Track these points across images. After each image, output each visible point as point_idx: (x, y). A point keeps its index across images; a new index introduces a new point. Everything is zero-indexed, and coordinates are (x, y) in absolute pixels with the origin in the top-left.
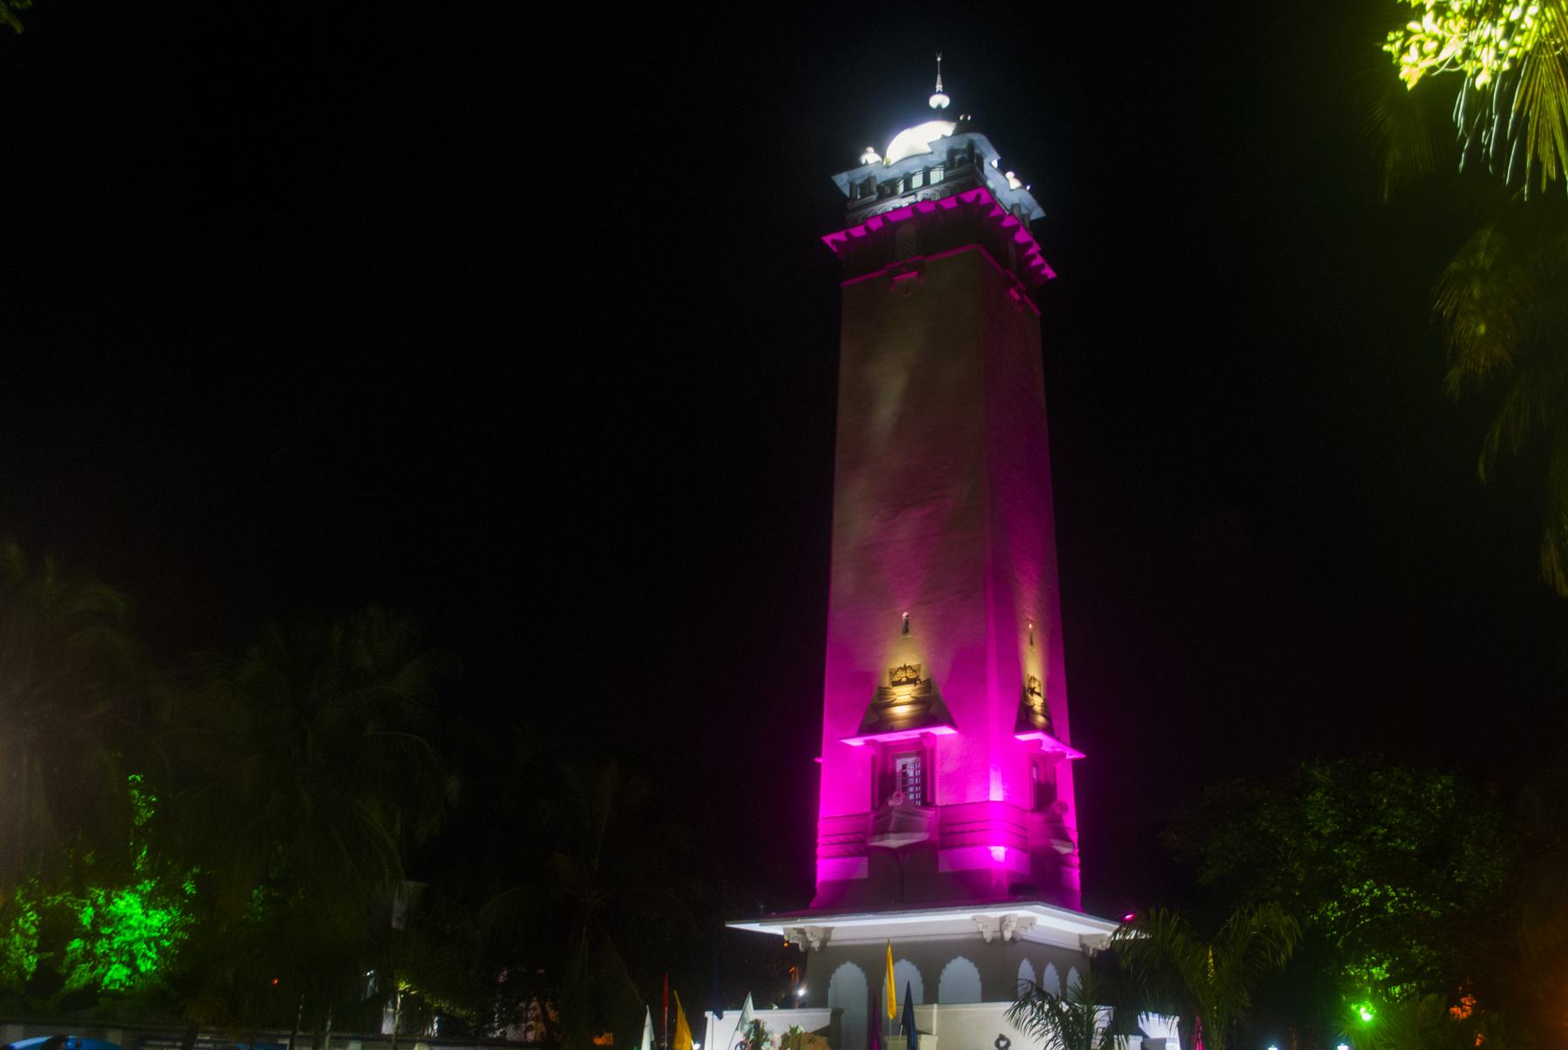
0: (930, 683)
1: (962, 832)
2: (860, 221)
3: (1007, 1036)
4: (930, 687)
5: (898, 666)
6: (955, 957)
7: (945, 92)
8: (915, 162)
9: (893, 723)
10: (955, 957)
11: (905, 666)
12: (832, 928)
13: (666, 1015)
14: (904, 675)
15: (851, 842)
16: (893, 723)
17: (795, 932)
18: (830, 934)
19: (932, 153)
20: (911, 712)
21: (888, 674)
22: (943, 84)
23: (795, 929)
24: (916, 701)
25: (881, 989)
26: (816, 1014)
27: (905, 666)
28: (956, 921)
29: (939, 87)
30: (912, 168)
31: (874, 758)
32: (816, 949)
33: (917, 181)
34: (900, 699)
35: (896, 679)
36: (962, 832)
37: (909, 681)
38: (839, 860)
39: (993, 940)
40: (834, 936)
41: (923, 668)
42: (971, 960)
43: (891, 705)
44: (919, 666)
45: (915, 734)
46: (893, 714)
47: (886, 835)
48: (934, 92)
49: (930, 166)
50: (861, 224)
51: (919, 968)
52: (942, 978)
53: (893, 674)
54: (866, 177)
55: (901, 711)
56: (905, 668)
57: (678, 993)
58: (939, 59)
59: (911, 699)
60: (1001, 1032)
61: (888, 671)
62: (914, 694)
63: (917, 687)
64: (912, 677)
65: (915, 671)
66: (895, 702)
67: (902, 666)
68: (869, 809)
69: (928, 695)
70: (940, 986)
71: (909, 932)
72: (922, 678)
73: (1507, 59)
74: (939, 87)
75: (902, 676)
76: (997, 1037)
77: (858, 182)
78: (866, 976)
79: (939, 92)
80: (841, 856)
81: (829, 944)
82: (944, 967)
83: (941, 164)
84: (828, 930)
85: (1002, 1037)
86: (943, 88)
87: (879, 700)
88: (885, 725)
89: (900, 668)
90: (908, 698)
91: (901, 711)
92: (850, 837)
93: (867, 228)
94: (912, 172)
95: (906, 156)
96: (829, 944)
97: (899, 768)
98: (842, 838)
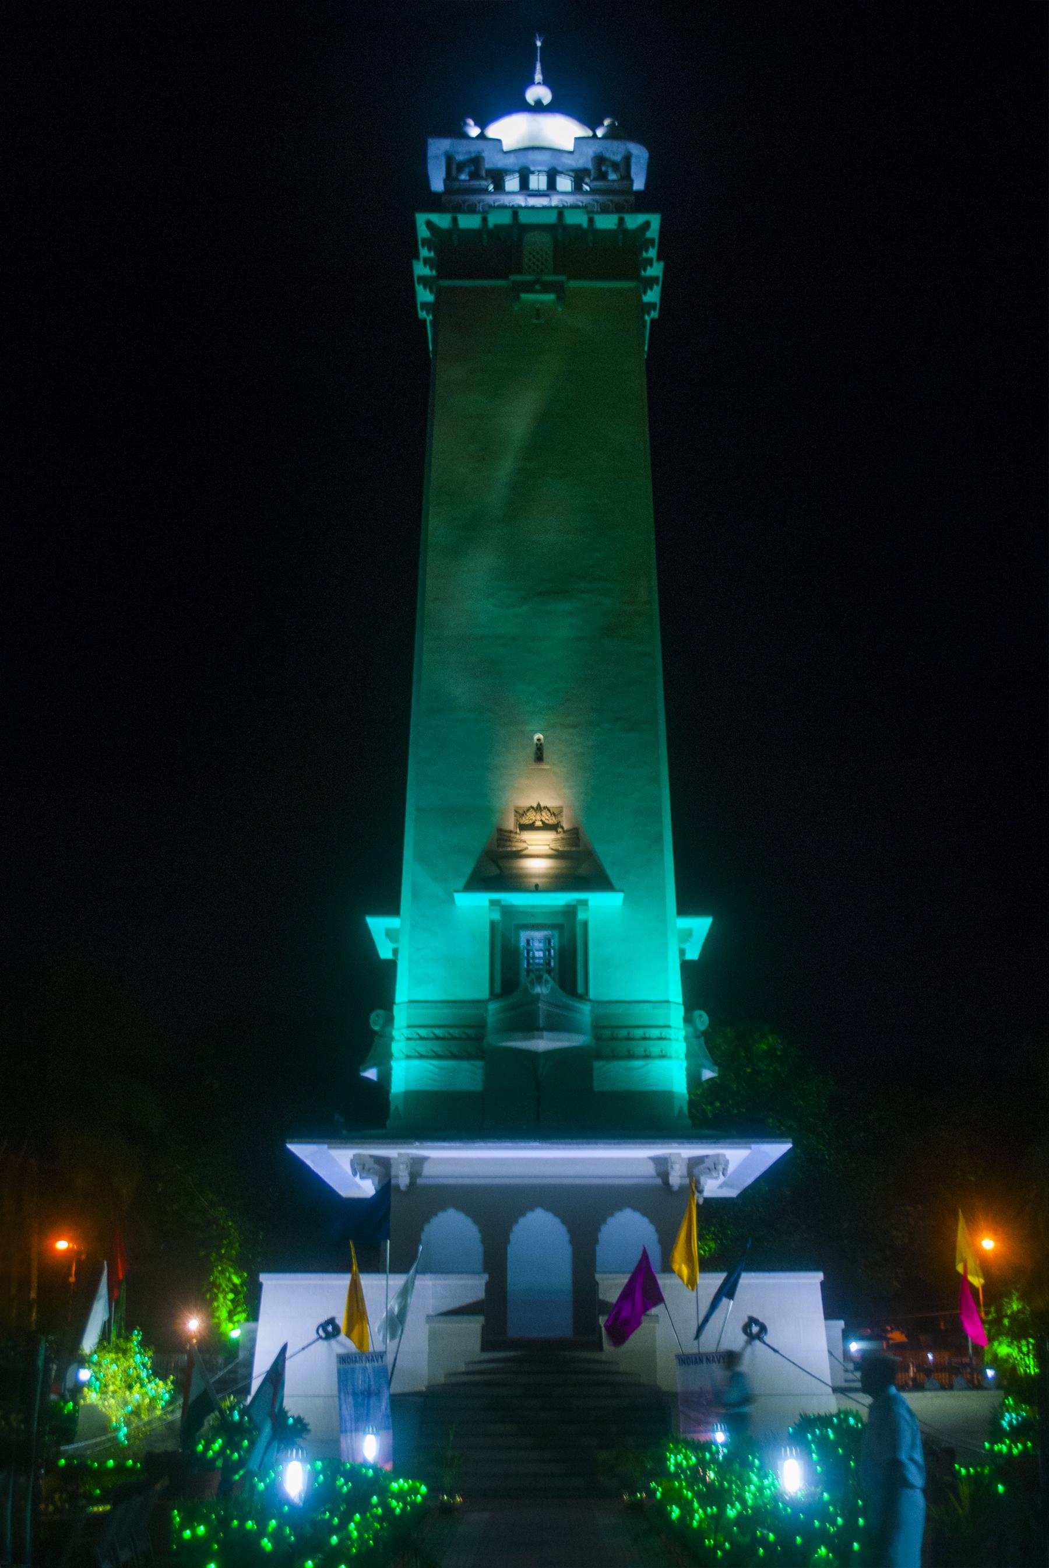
1: (644, 1039)
3: (761, 1319)
5: (529, 805)
7: (546, 83)
11: (539, 805)
14: (538, 818)
15: (422, 1038)
18: (422, 1168)
20: (551, 868)
23: (371, 1156)
24: (557, 855)
25: (506, 1249)
27: (539, 805)
29: (538, 77)
30: (535, 163)
31: (493, 925)
32: (403, 1188)
33: (537, 182)
34: (532, 849)
35: (525, 821)
36: (644, 1039)
37: (546, 827)
38: (435, 1062)
39: (680, 1188)
40: (428, 1170)
41: (566, 812)
43: (519, 855)
44: (561, 808)
46: (522, 868)
47: (536, 1033)
48: (531, 82)
49: (559, 169)
50: (479, 212)
53: (520, 813)
54: (473, 155)
55: (537, 866)
56: (539, 809)
59: (551, 852)
62: (553, 846)
63: (559, 836)
65: (554, 814)
66: (526, 852)
68: (485, 994)
69: (573, 849)
70: (598, 1248)
71: (623, 1170)
72: (566, 825)
74: (538, 77)
75: (537, 819)
76: (746, 1320)
77: (460, 158)
79: (539, 83)
80: (438, 1057)
81: (419, 1181)
83: (574, 171)
85: (752, 1321)
86: (543, 80)
90: (545, 849)
91: (537, 866)
92: (452, 1031)
93: (485, 220)
97: (523, 943)
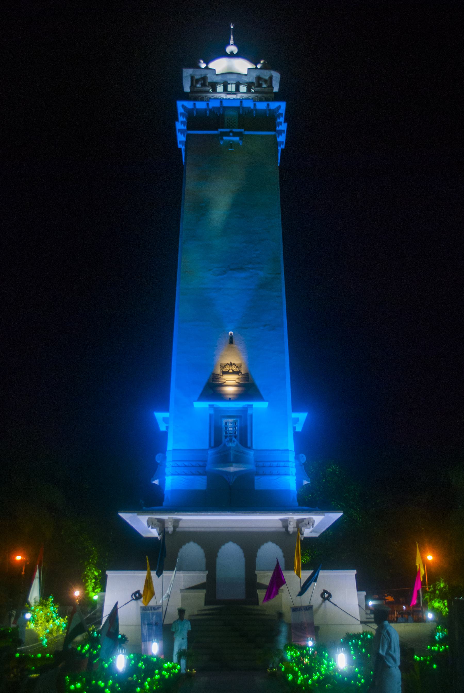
0: (248, 376)
2: (206, 99)
4: (248, 378)
5: (227, 363)
6: (267, 542)
7: (235, 44)
8: (234, 77)
9: (225, 396)
10: (227, 542)
11: (231, 363)
12: (180, 520)
13: (42, 572)
15: (179, 466)
16: (225, 396)
17: (156, 520)
19: (246, 75)
20: (236, 391)
21: (219, 367)
22: (234, 40)
23: (156, 519)
24: (239, 385)
26: (199, 574)
27: (231, 363)
28: (171, 517)
29: (232, 42)
30: (230, 80)
32: (170, 533)
33: (232, 88)
35: (225, 370)
36: (277, 466)
37: (234, 373)
40: (181, 525)
41: (243, 366)
42: (277, 544)
43: (222, 385)
45: (241, 404)
46: (222, 391)
48: (229, 44)
49: (241, 82)
51: (242, 548)
52: (258, 554)
55: (230, 390)
56: (231, 364)
57: (148, 557)
58: (232, 27)
60: (324, 589)
61: (219, 364)
62: (237, 381)
63: (240, 377)
64: (236, 370)
65: (237, 367)
66: (225, 384)
67: (229, 363)
68: (206, 446)
69: (246, 382)
71: (234, 525)
72: (243, 372)
73: (231, 130)
74: (232, 42)
75: (230, 369)
78: (205, 552)
80: (186, 474)
81: (177, 530)
82: (259, 547)
83: (247, 83)
84: (177, 521)
85: (325, 592)
87: (213, 381)
88: (221, 397)
89: (228, 364)
90: (233, 383)
91: (230, 390)
94: (229, 82)
95: (224, 72)
96: (177, 530)
98: (194, 463)
